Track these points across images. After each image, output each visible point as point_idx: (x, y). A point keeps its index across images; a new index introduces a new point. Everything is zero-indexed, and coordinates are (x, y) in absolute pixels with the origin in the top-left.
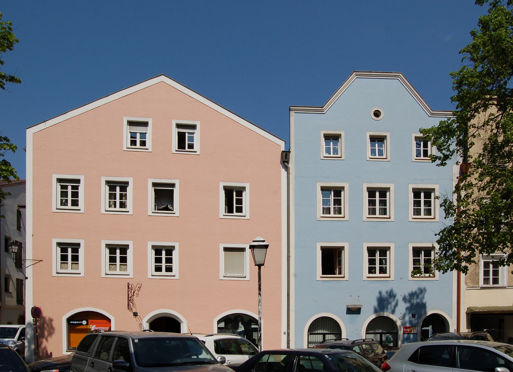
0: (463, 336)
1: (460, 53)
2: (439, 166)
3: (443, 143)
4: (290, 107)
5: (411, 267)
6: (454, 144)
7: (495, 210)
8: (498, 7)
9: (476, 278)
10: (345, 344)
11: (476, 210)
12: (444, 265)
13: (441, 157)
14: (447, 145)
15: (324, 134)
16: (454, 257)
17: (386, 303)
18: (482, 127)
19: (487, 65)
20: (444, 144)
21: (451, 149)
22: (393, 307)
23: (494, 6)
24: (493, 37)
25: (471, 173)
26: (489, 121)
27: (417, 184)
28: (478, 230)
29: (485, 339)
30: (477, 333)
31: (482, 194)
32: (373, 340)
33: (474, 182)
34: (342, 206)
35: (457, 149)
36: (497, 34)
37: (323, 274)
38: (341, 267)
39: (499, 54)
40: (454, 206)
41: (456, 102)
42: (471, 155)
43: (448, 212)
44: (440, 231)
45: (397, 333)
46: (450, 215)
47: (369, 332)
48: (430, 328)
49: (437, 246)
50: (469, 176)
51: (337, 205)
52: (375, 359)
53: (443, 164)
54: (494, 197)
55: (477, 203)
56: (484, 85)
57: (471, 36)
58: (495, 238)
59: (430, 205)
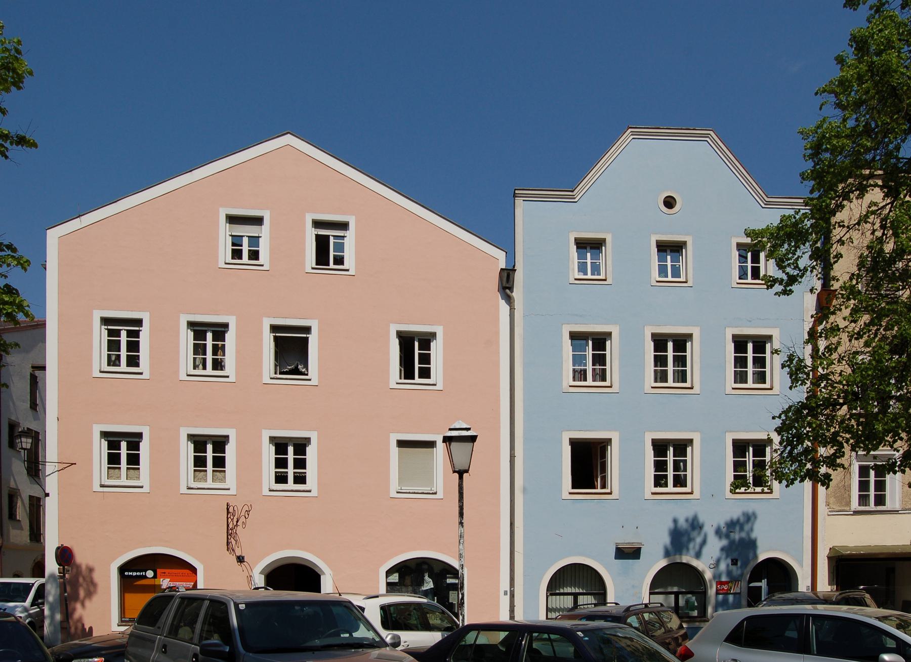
0: (822, 598)
1: (816, 94)
2: (779, 296)
3: (787, 254)
4: (515, 190)
5: (730, 475)
6: (807, 256)
7: (879, 373)
8: (885, 12)
9: (846, 495)
10: (613, 612)
11: (845, 374)
12: (788, 472)
13: (783, 279)
14: (794, 258)
15: (576, 239)
16: (806, 457)
17: (685, 539)
18: (856, 226)
19: (864, 116)
20: (789, 256)
21: (801, 266)
22: (697, 547)
23: (877, 11)
24: (875, 66)
25: (837, 308)
26: (869, 215)
27: (740, 327)
28: (850, 409)
29: (860, 602)
30: (847, 592)
31: (856, 345)
32: (662, 605)
33: (842, 324)
34: (608, 367)
35: (812, 265)
36: (883, 60)
37: (573, 487)
38: (605, 475)
39: (886, 95)
40: (806, 366)
41: (809, 181)
42: (836, 277)
43: (796, 377)
44: (782, 412)
45: (705, 593)
46: (800, 382)
47: (656, 591)
48: (763, 584)
49: (776, 439)
50: (834, 313)
51: (598, 365)
52: (666, 638)
53: (786, 292)
54: (878, 351)
55: (846, 362)
56: (860, 151)
57: (837, 64)
58: (880, 423)
59: (763, 365)
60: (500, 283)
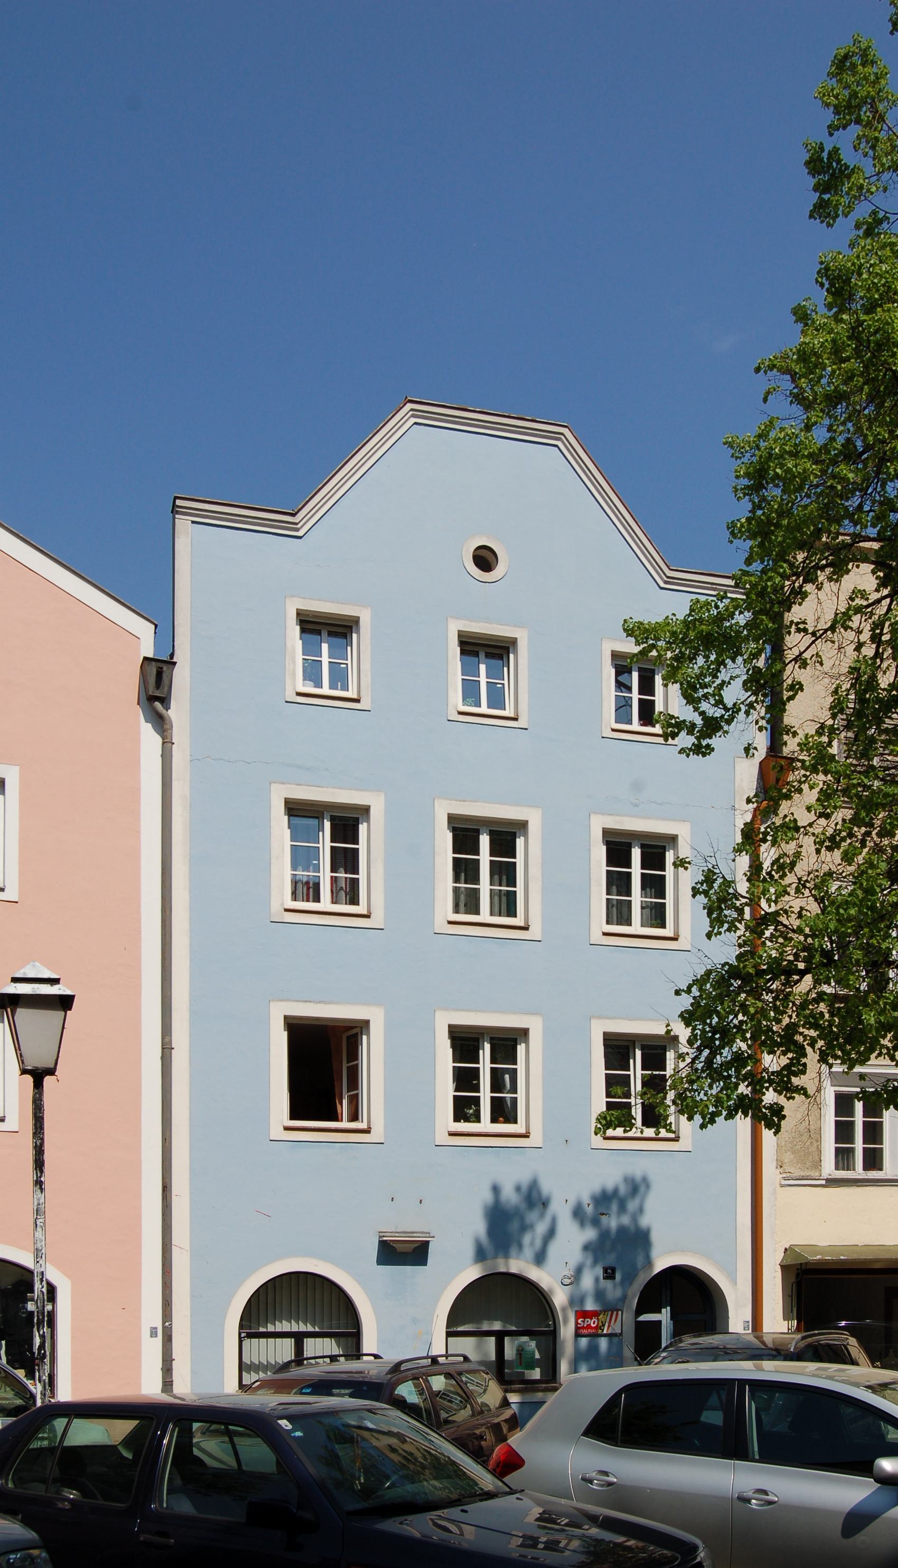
0: (770, 1345)
1: (758, 370)
2: (688, 756)
3: (702, 675)
4: (176, 498)
5: (599, 1102)
6: (738, 683)
7: (869, 913)
8: (882, 236)
9: (813, 1149)
10: (370, 1373)
11: (809, 914)
12: (705, 1098)
13: (695, 724)
14: (715, 685)
15: (299, 613)
16: (738, 1071)
17: (514, 1226)
18: (829, 632)
19: (844, 423)
20: (706, 680)
21: (729, 701)
22: (538, 1243)
23: (869, 233)
24: (864, 330)
25: (794, 787)
26: (851, 612)
27: (617, 815)
28: (817, 982)
29: (839, 1355)
30: (815, 1335)
31: (828, 859)
32: (466, 1359)
33: (804, 819)
34: (362, 876)
35: (749, 700)
36: (877, 321)
37: (293, 1116)
38: (357, 1094)
39: (882, 389)
40: (736, 896)
41: (745, 540)
42: (792, 727)
43: (719, 915)
44: (693, 980)
45: (553, 1334)
46: (726, 926)
47: (460, 1329)
48: (664, 1316)
49: (683, 1032)
50: (788, 797)
51: (342, 870)
52: (477, 1427)
53: (701, 750)
54: (866, 872)
55: (810, 892)
56: (836, 487)
57: (796, 322)
58: (871, 1010)
59: (661, 894)
60: (142, 681)
